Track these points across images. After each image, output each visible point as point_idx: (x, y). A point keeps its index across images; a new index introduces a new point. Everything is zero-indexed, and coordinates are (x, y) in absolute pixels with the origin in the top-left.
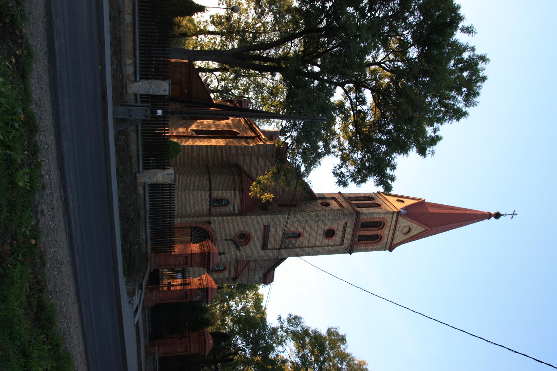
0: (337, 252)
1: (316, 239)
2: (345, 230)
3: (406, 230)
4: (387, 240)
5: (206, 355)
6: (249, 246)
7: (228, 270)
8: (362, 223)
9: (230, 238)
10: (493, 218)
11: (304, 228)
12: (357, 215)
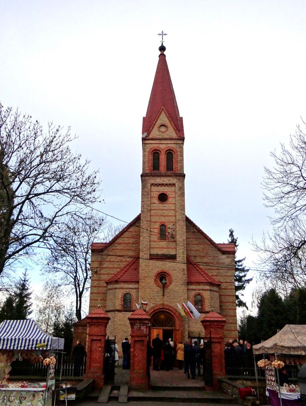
1: (168, 210)
2: (160, 184)
3: (163, 129)
6: (171, 272)
7: (201, 291)
9: (162, 292)
10: (165, 53)
11: (155, 222)
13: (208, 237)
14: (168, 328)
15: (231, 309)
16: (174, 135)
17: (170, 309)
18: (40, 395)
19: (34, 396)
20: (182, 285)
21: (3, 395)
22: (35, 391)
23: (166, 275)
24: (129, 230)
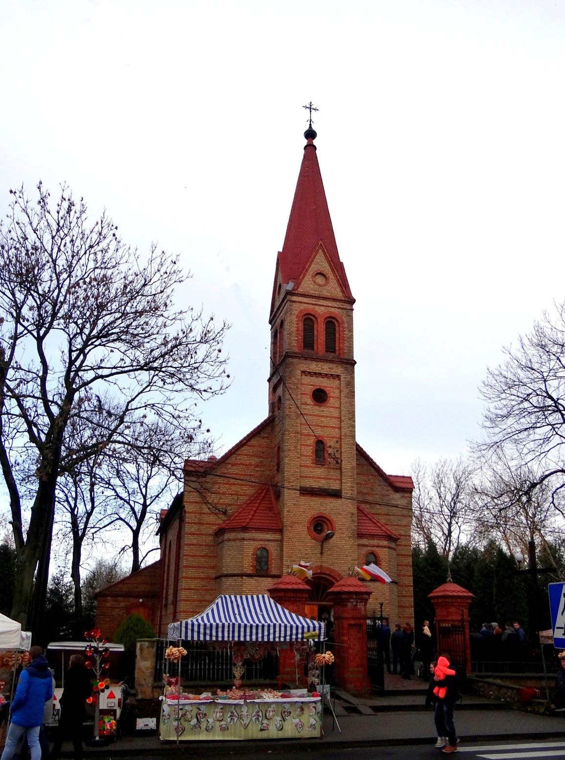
0: (351, 384)
1: (327, 417)
2: (315, 373)
3: (320, 280)
4: (334, 307)
5: (471, 594)
6: (334, 518)
8: (305, 347)
10: (315, 142)
12: (291, 357)
13: (375, 463)
14: (326, 603)
15: (404, 575)
16: (339, 294)
17: (332, 575)
18: (311, 707)
19: (302, 709)
20: (350, 537)
21: (256, 710)
22: (302, 703)
23: (325, 522)
24: (249, 443)
